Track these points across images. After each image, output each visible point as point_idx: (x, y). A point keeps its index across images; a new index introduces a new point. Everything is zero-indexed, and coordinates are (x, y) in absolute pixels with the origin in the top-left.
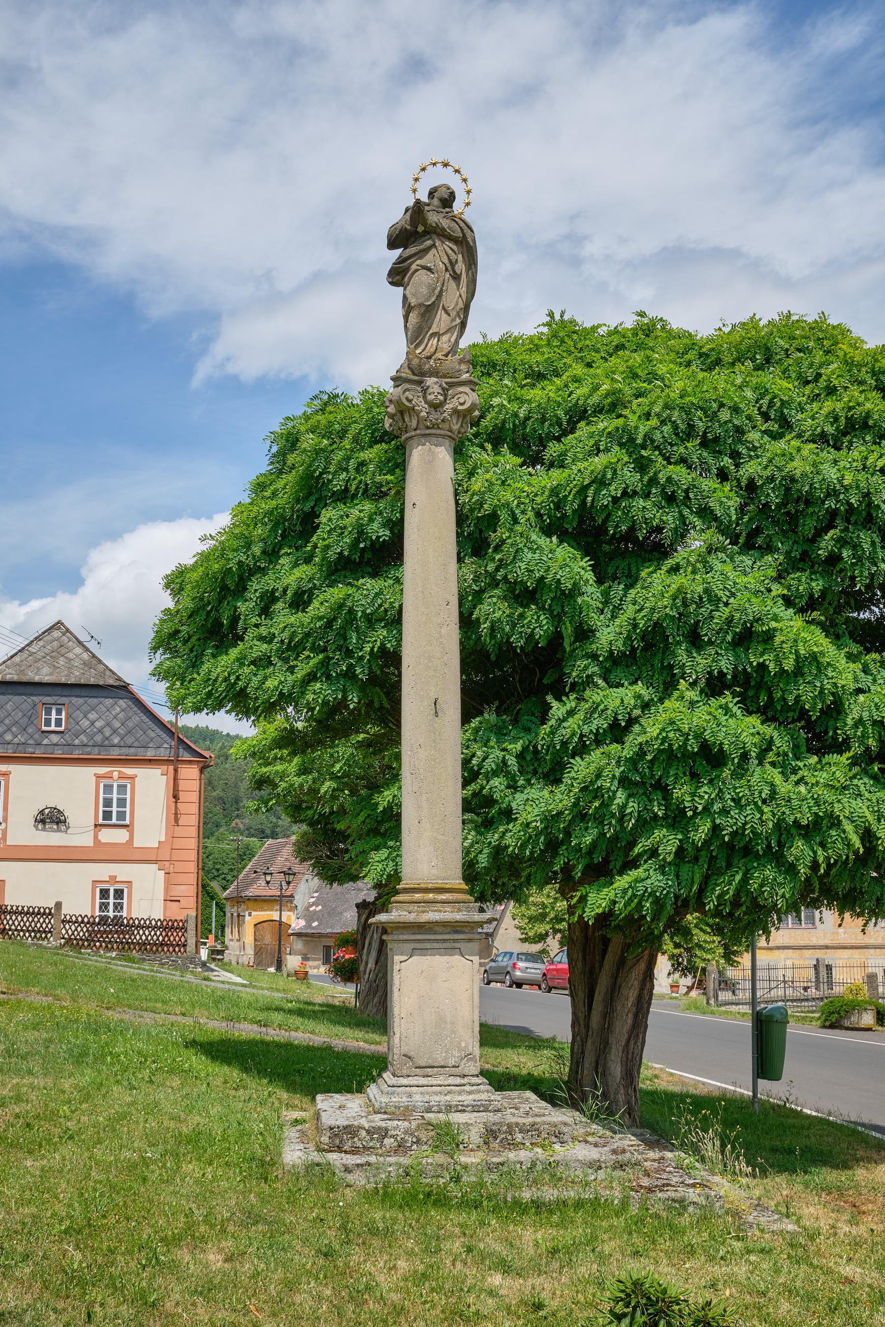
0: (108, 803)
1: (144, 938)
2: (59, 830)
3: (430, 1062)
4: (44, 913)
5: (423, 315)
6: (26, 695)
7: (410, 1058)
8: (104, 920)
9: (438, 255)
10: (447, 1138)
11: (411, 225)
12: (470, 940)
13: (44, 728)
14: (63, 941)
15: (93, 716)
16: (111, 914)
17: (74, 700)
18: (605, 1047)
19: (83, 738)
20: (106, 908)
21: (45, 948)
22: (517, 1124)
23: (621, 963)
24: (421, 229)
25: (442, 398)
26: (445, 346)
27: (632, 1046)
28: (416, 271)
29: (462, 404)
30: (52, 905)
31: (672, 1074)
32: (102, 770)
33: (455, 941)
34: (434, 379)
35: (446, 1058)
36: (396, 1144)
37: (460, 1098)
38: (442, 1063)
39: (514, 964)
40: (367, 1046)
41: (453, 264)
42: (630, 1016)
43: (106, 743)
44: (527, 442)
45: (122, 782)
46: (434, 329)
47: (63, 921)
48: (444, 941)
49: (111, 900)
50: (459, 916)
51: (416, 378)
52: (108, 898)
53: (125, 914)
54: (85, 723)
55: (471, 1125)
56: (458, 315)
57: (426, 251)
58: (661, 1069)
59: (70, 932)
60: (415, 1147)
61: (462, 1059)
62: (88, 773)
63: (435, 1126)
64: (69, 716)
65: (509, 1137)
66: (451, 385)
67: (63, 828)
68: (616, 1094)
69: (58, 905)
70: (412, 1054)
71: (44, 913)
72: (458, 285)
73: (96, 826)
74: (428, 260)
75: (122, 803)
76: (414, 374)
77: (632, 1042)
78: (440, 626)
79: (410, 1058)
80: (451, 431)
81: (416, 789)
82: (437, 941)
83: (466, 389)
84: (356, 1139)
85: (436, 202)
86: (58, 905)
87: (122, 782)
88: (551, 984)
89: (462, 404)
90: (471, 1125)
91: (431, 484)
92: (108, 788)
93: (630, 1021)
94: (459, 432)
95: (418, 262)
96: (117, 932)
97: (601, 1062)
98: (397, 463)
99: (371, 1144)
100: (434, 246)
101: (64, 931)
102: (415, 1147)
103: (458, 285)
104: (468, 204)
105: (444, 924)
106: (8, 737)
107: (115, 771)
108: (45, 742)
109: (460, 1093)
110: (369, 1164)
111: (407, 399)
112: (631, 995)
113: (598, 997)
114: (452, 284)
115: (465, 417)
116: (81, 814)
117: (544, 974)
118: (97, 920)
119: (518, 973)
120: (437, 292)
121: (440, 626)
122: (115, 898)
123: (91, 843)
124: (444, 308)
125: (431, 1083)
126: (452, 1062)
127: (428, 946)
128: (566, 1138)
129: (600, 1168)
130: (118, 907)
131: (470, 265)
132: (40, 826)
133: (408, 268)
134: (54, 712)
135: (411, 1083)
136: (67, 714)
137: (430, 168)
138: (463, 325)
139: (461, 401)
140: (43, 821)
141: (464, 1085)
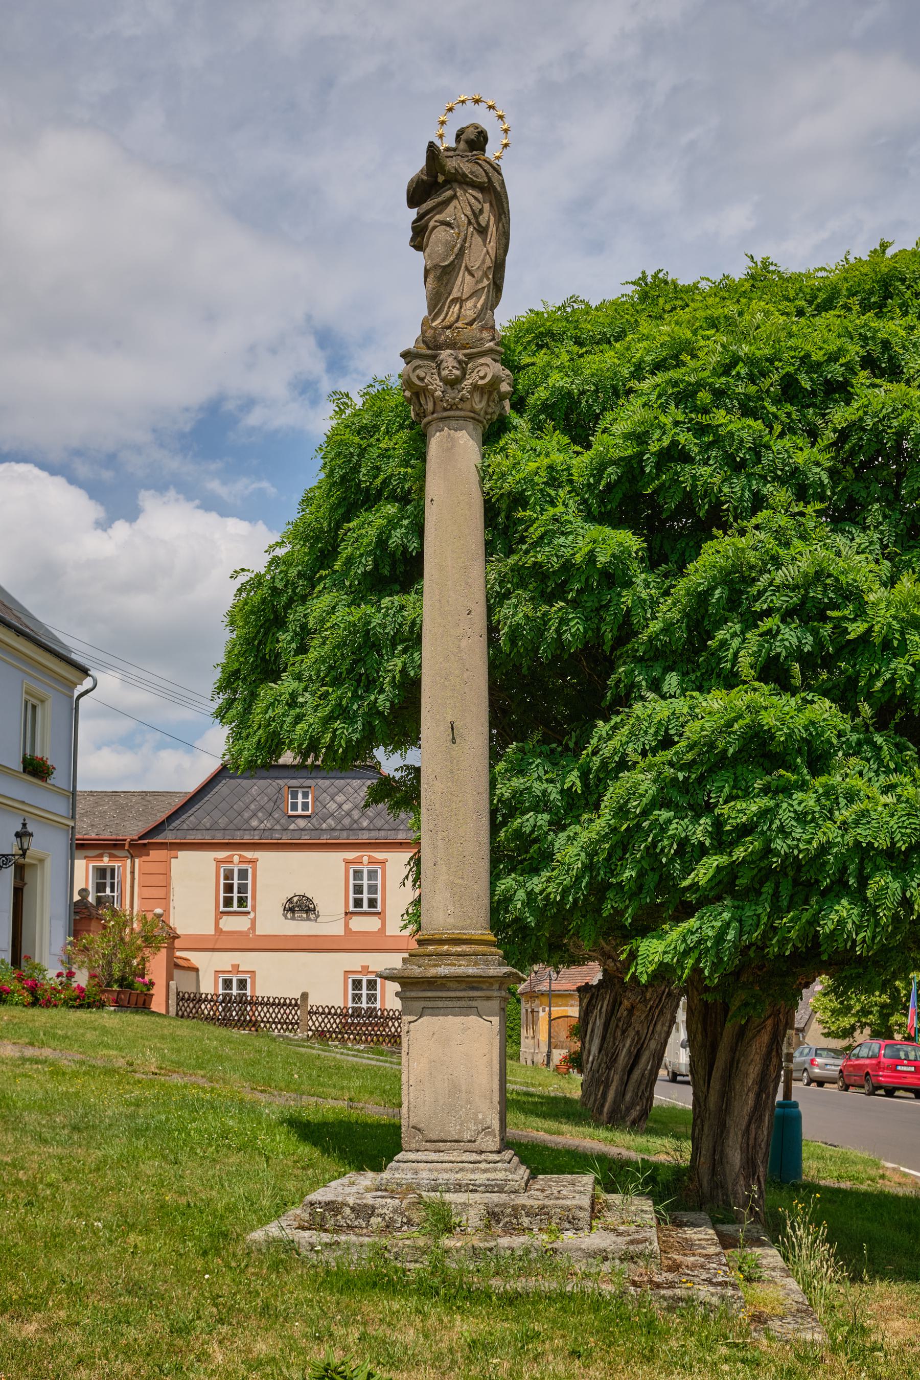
0: (358, 889)
1: (393, 1030)
2: (308, 919)
3: (443, 1136)
4: (290, 1004)
5: (439, 279)
6: (271, 778)
7: (419, 1130)
8: (357, 1012)
9: (462, 206)
10: (444, 1222)
11: (428, 175)
12: (488, 998)
13: (291, 813)
14: (310, 1033)
15: (340, 798)
16: (364, 1005)
17: (321, 782)
18: (722, 1132)
19: (331, 821)
20: (360, 999)
21: (291, 1040)
22: (524, 1207)
23: (742, 1032)
24: (441, 178)
25: (457, 372)
26: (468, 313)
27: (753, 1132)
28: (435, 227)
29: (482, 378)
30: (298, 996)
31: (905, 1175)
32: (351, 855)
33: (471, 998)
34: (449, 351)
35: (460, 1132)
36: (383, 1224)
37: (472, 1177)
38: (456, 1137)
39: (812, 1060)
40: (547, 1137)
41: (477, 215)
42: (752, 1096)
43: (355, 826)
44: (574, 418)
45: (372, 867)
46: (455, 294)
47: (310, 1013)
48: (459, 998)
49: (364, 992)
50: (471, 971)
51: (430, 352)
52: (360, 989)
53: (378, 1005)
54: (332, 806)
55: (470, 1208)
56: (485, 275)
57: (446, 203)
58: (894, 1169)
59: (317, 1024)
60: (405, 1228)
61: (479, 1133)
62: (335, 860)
63: (427, 1206)
64: (315, 799)
65: (514, 1221)
66: (471, 357)
67: (313, 916)
68: (735, 1184)
69: (305, 996)
70: (421, 1126)
71: (290, 1004)
72: (484, 241)
73: (346, 914)
74: (447, 215)
75: (373, 889)
76: (429, 348)
77: (753, 1126)
78: (459, 638)
79: (419, 1130)
80: (474, 412)
81: (431, 827)
82: (451, 999)
83: (487, 360)
84: (339, 1217)
85: (462, 145)
86: (305, 996)
87: (372, 867)
88: (848, 1082)
89: (482, 378)
90: (470, 1208)
91: (455, 471)
92: (358, 874)
93: (751, 1102)
94: (486, 413)
95: (437, 217)
96: (371, 1024)
97: (719, 1149)
98: (418, 450)
99: (356, 1223)
100: (455, 196)
101: (310, 1023)
102: (405, 1228)
103: (484, 241)
104: (506, 145)
105: (459, 980)
106: (254, 823)
107: (366, 855)
108: (292, 827)
109: (473, 1171)
110: (337, 1243)
111: (418, 377)
112: (752, 1071)
113: (716, 1074)
114: (477, 239)
115: (490, 393)
116: (331, 899)
117: (841, 1071)
118: (350, 1011)
119: (817, 1070)
120: (456, 250)
121: (459, 638)
122: (368, 989)
123: (342, 932)
124: (467, 268)
125: (441, 1159)
126: (467, 1136)
127: (440, 1004)
128: (581, 1224)
129: (606, 1259)
130: (371, 998)
131: (500, 215)
132: (289, 915)
133: (426, 226)
134: (300, 795)
135: (419, 1158)
136: (313, 797)
137: (470, 104)
138: (497, 287)
139: (482, 374)
140: (292, 910)
141: (479, 1162)
